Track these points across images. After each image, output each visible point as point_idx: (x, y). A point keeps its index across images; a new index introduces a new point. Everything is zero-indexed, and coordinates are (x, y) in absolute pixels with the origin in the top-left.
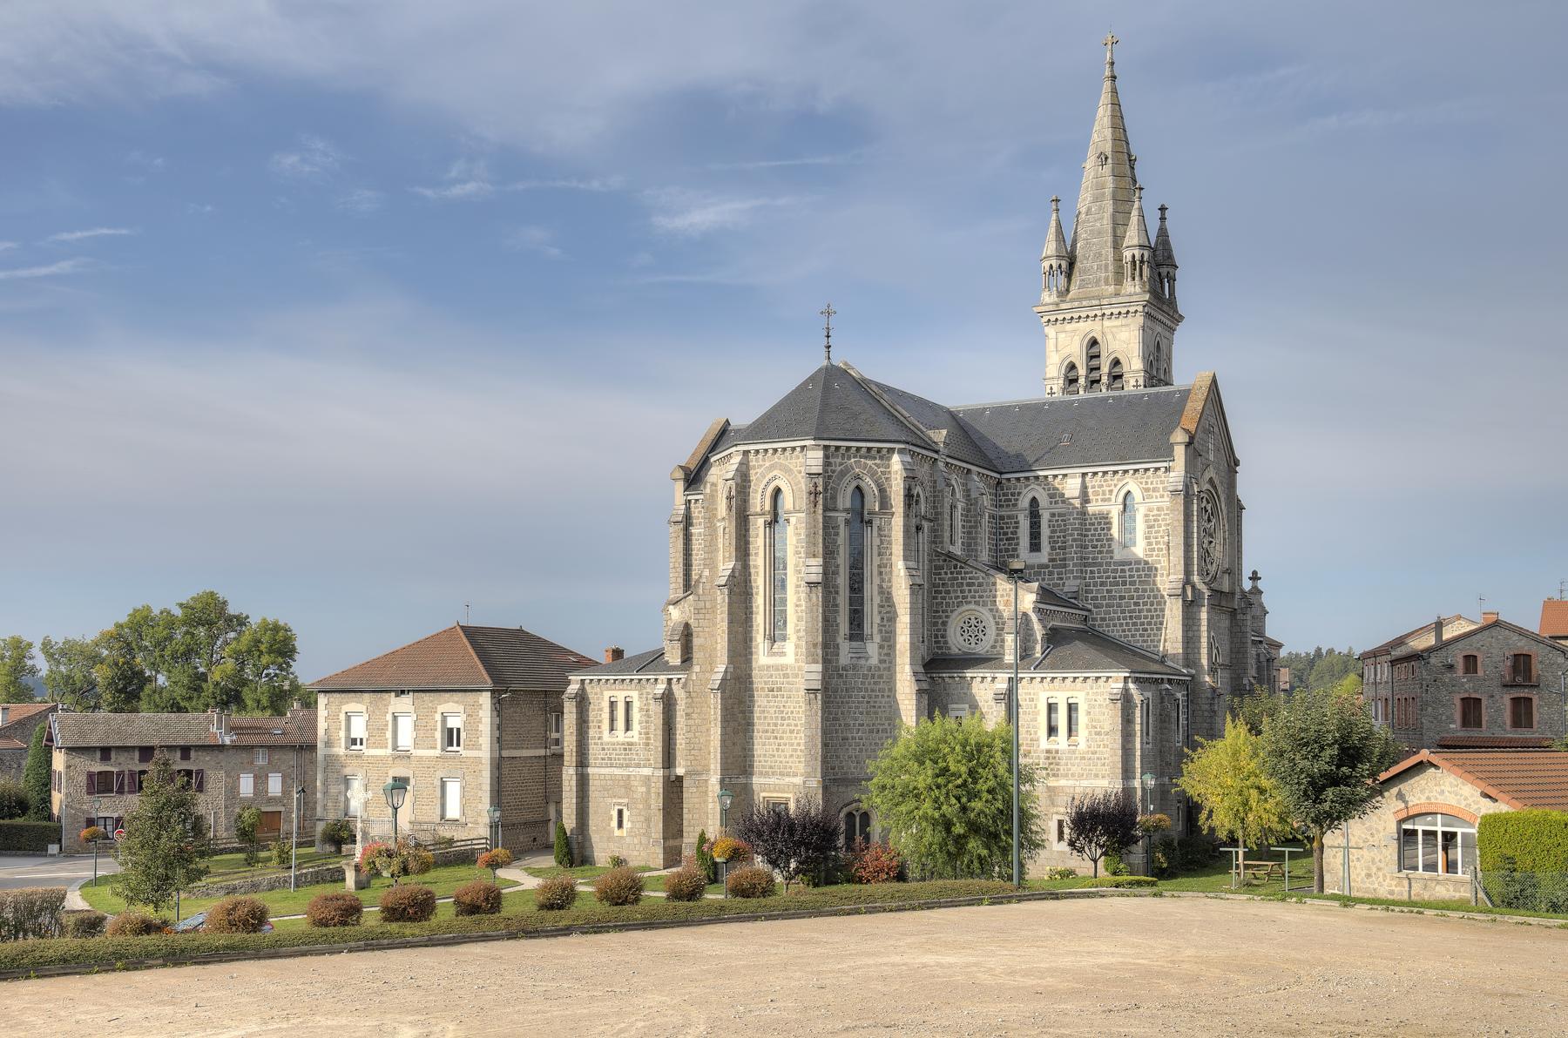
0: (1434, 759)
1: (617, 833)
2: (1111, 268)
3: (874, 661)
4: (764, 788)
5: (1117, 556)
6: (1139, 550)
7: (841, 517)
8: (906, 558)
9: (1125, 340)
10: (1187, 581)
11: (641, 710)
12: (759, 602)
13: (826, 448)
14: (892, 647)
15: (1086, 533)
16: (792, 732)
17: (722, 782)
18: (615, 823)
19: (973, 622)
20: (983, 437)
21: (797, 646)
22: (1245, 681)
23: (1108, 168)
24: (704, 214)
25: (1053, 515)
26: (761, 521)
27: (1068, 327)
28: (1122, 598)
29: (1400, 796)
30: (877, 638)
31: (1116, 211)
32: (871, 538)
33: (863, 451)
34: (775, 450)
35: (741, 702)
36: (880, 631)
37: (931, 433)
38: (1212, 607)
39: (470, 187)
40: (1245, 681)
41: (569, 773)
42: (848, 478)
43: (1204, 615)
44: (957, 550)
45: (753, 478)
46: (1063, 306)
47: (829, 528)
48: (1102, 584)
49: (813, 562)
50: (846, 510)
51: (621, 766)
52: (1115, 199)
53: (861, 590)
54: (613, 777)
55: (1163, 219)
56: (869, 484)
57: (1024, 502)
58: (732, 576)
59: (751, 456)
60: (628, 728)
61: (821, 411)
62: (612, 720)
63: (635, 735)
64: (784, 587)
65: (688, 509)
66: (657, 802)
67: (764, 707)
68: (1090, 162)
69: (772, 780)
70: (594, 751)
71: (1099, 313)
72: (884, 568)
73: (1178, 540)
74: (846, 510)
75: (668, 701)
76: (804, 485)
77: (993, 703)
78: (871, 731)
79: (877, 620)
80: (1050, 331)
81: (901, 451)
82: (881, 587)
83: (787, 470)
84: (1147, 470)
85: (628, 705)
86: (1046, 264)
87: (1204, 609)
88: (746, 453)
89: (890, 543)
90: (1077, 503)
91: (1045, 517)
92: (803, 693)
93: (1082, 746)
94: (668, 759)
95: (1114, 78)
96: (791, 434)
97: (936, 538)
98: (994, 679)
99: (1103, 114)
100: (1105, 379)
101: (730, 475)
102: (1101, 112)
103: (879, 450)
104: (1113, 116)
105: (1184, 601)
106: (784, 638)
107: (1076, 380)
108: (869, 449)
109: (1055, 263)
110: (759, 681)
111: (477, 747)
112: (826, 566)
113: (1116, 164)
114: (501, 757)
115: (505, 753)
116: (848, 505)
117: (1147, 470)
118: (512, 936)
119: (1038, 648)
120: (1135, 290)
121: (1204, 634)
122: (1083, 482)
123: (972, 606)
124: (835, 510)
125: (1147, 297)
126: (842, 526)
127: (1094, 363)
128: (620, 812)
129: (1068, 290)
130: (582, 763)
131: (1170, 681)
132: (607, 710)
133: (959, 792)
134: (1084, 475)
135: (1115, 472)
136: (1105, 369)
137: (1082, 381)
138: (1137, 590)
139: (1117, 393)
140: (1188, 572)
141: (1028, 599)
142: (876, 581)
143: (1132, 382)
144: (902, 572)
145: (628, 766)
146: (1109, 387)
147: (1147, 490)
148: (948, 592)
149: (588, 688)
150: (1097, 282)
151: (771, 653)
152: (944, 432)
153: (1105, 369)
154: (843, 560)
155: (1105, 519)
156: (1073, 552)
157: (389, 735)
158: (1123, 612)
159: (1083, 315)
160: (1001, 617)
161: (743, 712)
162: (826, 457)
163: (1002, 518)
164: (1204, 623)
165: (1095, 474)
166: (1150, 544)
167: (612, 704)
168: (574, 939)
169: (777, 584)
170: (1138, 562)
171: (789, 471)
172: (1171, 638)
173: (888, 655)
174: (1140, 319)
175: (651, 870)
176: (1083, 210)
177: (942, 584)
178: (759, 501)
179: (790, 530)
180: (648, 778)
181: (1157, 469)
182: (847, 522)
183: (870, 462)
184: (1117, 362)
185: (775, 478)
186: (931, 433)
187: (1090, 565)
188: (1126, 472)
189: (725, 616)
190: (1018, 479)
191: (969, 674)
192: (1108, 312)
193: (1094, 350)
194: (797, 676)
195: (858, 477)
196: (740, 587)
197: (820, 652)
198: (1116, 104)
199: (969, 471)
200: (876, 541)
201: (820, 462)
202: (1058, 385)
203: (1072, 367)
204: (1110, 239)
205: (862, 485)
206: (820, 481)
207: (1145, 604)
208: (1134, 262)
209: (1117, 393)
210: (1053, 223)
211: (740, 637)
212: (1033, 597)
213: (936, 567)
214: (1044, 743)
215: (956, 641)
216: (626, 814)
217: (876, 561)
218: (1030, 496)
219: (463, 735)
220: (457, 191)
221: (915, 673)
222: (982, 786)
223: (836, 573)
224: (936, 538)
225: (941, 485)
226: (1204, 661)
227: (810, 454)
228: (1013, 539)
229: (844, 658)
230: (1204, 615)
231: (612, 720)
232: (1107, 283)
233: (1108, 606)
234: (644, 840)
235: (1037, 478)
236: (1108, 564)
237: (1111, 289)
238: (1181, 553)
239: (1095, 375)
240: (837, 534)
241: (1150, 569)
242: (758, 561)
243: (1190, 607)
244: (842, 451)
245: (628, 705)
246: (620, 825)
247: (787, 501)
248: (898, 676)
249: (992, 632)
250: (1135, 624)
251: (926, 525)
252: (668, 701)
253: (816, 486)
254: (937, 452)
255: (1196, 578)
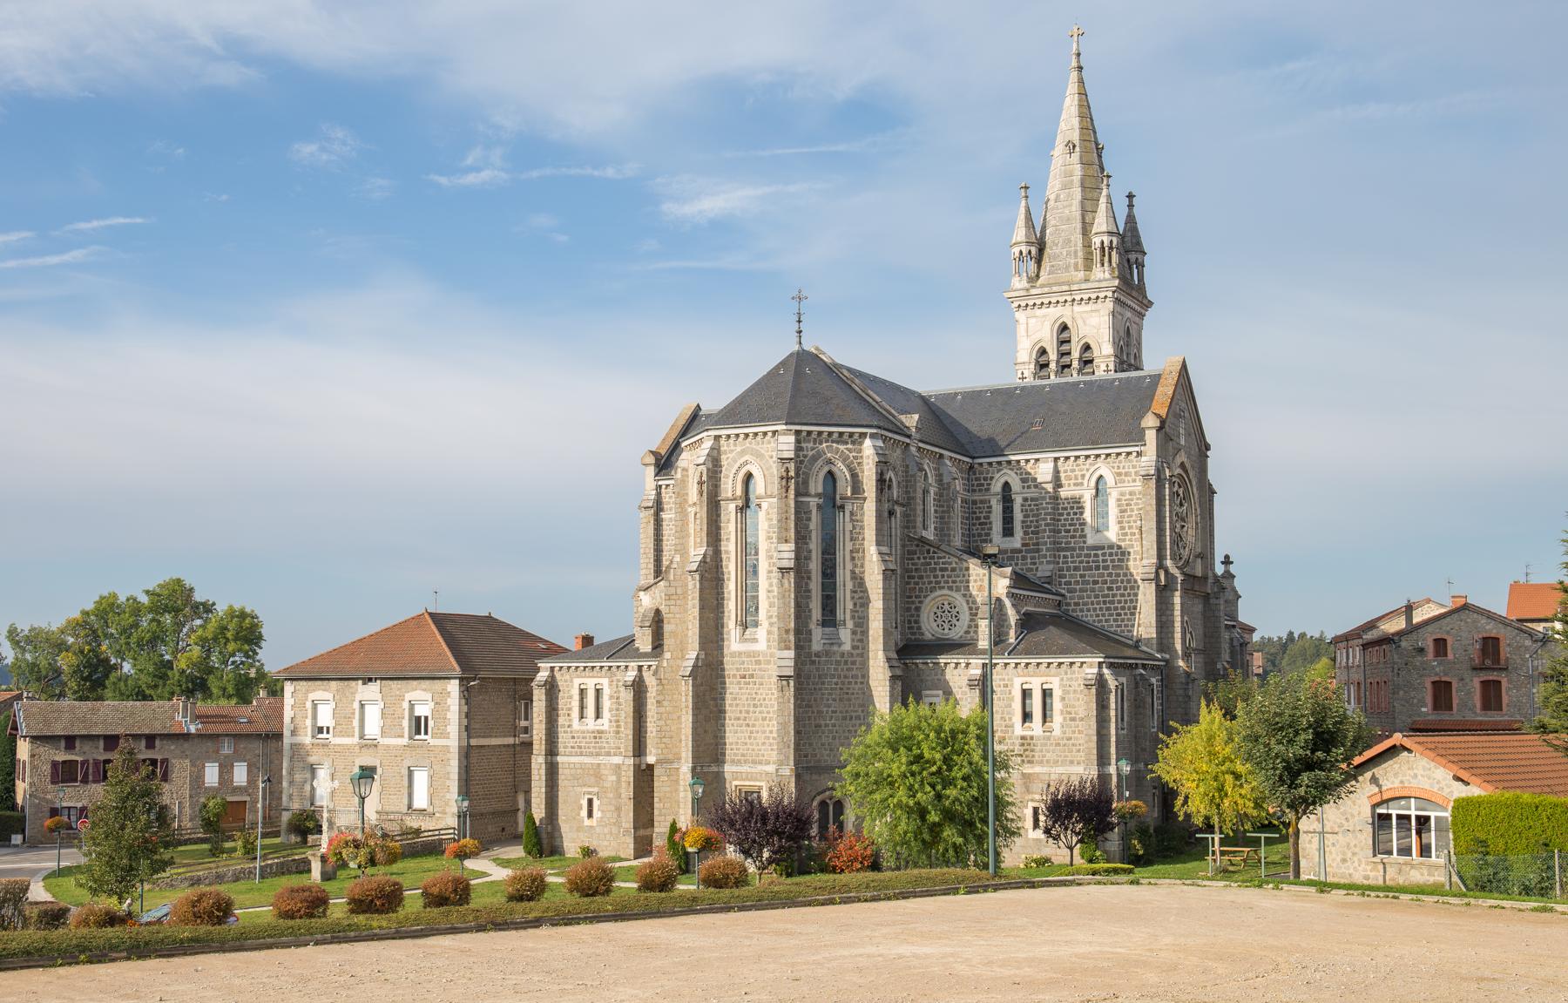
0: (1407, 742)
1: (587, 822)
2: (1080, 254)
3: (847, 647)
4: (736, 776)
5: (1090, 541)
6: (1112, 535)
7: (813, 502)
8: (878, 543)
9: (1095, 326)
10: (1160, 565)
11: (611, 697)
12: (731, 587)
13: (798, 433)
14: (865, 633)
15: (1057, 517)
16: (764, 719)
17: (694, 769)
18: (584, 813)
19: (947, 607)
20: (954, 422)
21: (769, 633)
22: (1219, 666)
23: (1076, 156)
24: (717, 201)
25: (1025, 500)
26: (732, 506)
27: (1038, 312)
28: (1096, 582)
29: (1374, 780)
30: (850, 624)
31: (1084, 199)
32: (843, 523)
33: (835, 436)
34: (747, 435)
35: (712, 689)
36: (853, 617)
37: (902, 418)
38: (1185, 591)
39: (486, 175)
40: (1219, 666)
41: (538, 762)
42: (820, 463)
43: (1177, 600)
44: (930, 534)
45: (724, 462)
46: (1033, 291)
47: (801, 513)
48: (1076, 569)
49: (785, 547)
50: (818, 495)
51: (591, 755)
52: (1083, 186)
53: (833, 575)
54: (582, 766)
55: (1131, 206)
56: (841, 468)
57: (997, 487)
58: (703, 561)
59: (722, 441)
60: (598, 716)
61: (793, 397)
62: (582, 708)
63: (605, 723)
64: (755, 573)
65: (659, 494)
66: (627, 792)
67: (736, 695)
68: (1059, 150)
69: (745, 768)
70: (563, 738)
71: (1069, 298)
72: (857, 553)
73: (1152, 524)
74: (818, 495)
75: (639, 688)
76: (775, 470)
77: (967, 689)
78: (844, 718)
79: (850, 605)
80: (1020, 316)
81: (873, 436)
82: (853, 572)
83: (759, 455)
84: (1118, 454)
85: (598, 692)
86: (1016, 250)
87: (1178, 594)
88: (717, 438)
89: (862, 528)
90: (1049, 487)
91: (1018, 501)
92: (775, 679)
93: (1057, 732)
94: (639, 748)
95: (1080, 68)
96: (762, 419)
97: (908, 522)
98: (968, 665)
99: (1071, 104)
100: (1075, 364)
101: (701, 460)
102: (1068, 101)
103: (851, 435)
104: (1080, 106)
105: (1157, 586)
106: (756, 624)
107: (1069, 366)
108: (841, 434)
109: (1025, 249)
110: (730, 667)
111: (445, 736)
112: (798, 551)
113: (1084, 152)
114: (469, 745)
115: (474, 742)
116: (820, 490)
117: (1118, 454)
118: (481, 928)
119: (1012, 633)
120: (1104, 276)
121: (1178, 619)
122: (1056, 467)
123: (945, 592)
124: (807, 494)
125: (1116, 282)
126: (814, 511)
127: (1065, 348)
128: (590, 802)
129: (1038, 276)
130: (552, 751)
131: (1144, 666)
132: (577, 697)
133: (934, 779)
134: (1056, 459)
135: (1087, 457)
136: (1076, 354)
137: (1053, 366)
138: (1110, 575)
139: (1088, 378)
140: (1161, 556)
141: (1002, 585)
142: (849, 566)
143: (1103, 367)
144: (875, 557)
145: (598, 754)
146: (1080, 371)
147: (1119, 474)
148: (921, 577)
149: (558, 675)
150: (1067, 268)
151: (743, 640)
152: (916, 417)
153: (1076, 354)
154: (815, 545)
155: (1077, 503)
156: (1046, 537)
157: (356, 723)
158: (1097, 596)
159: (1054, 300)
160: (974, 602)
161: (715, 699)
162: (798, 441)
163: (974, 502)
164: (1178, 607)
165: (1067, 458)
166: (1122, 528)
167: (582, 692)
168: (544, 931)
169: (749, 570)
170: (1111, 547)
171: (762, 456)
172: (1145, 624)
173: (861, 641)
174: (1110, 305)
175: (621, 860)
176: (1052, 197)
177: (915, 570)
178: (730, 486)
179: (762, 515)
180: (618, 766)
181: (1129, 454)
182: (819, 507)
183: (842, 447)
184: (1087, 347)
185: (746, 463)
186: (902, 418)
187: (1064, 549)
188: (1098, 456)
189: (697, 602)
190: (990, 464)
191: (942, 660)
192: (1078, 298)
193: (1065, 335)
194: (769, 662)
195: (829, 462)
196: (711, 573)
197: (792, 638)
198: (1083, 94)
199: (941, 456)
200: (849, 527)
201: (792, 447)
202: (1029, 370)
203: (1043, 352)
204: (1079, 226)
205: (834, 469)
206: (792, 466)
207: (1118, 588)
208: (1103, 248)
209: (1088, 378)
210: (1022, 210)
211: (711, 623)
212: (1007, 582)
213: (909, 552)
214: (576, 724)
215: (930, 627)
216: (596, 803)
217: (849, 546)
218: (1002, 481)
219: (431, 723)
220: (471, 179)
221: (888, 660)
222: (957, 773)
223: (808, 558)
224: (908, 522)
225: (913, 469)
226: (1178, 646)
227: (782, 439)
228: (986, 524)
229: (817, 644)
230: (1177, 600)
231: (582, 708)
232: (1076, 269)
233: (1082, 590)
234: (614, 830)
235: (1009, 462)
236: (1082, 549)
237: (1081, 275)
238: (1154, 537)
239: (1065, 360)
240: (809, 519)
241: (1123, 554)
242: (729, 547)
243: (1163, 593)
244: (814, 436)
245: (598, 692)
246: (590, 814)
247: (759, 486)
248: (871, 662)
249: (965, 617)
250: (1108, 609)
251: (898, 509)
252: (639, 688)
253: (787, 470)
254: (909, 437)
255: (1169, 563)
